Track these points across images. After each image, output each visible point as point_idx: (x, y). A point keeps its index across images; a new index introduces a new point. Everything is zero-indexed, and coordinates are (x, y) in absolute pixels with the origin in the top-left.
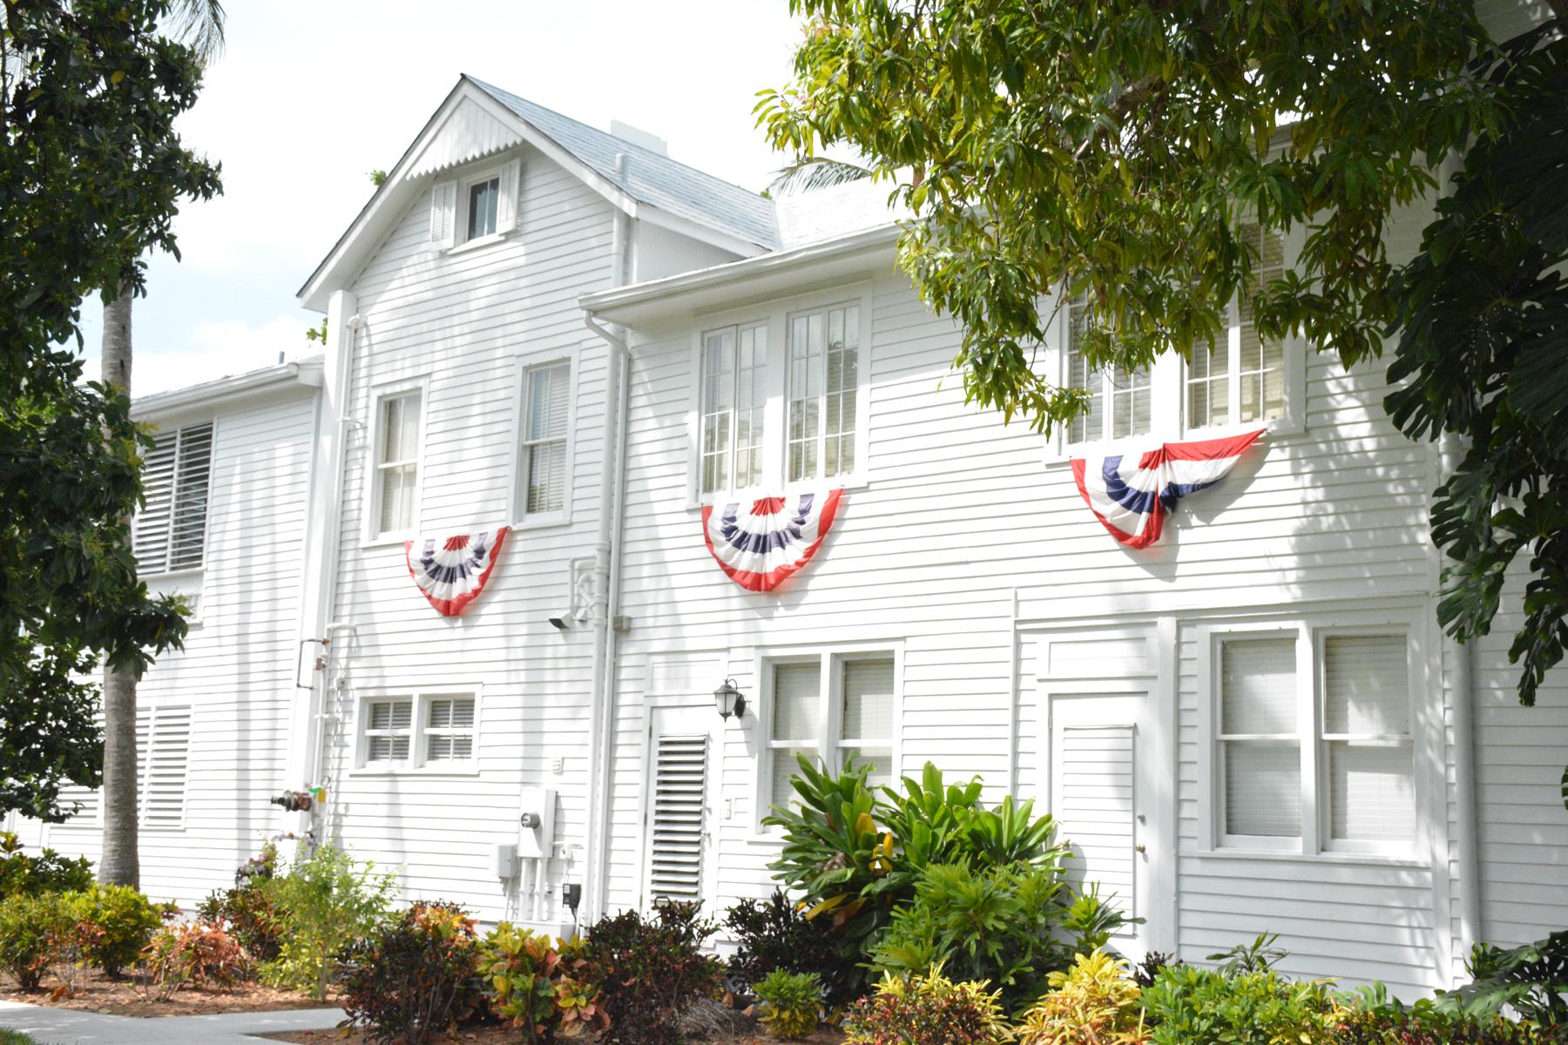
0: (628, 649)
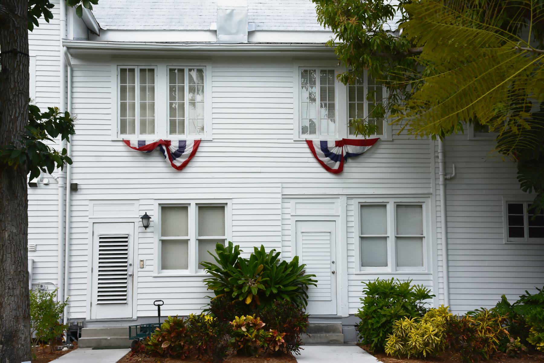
0: (76, 197)
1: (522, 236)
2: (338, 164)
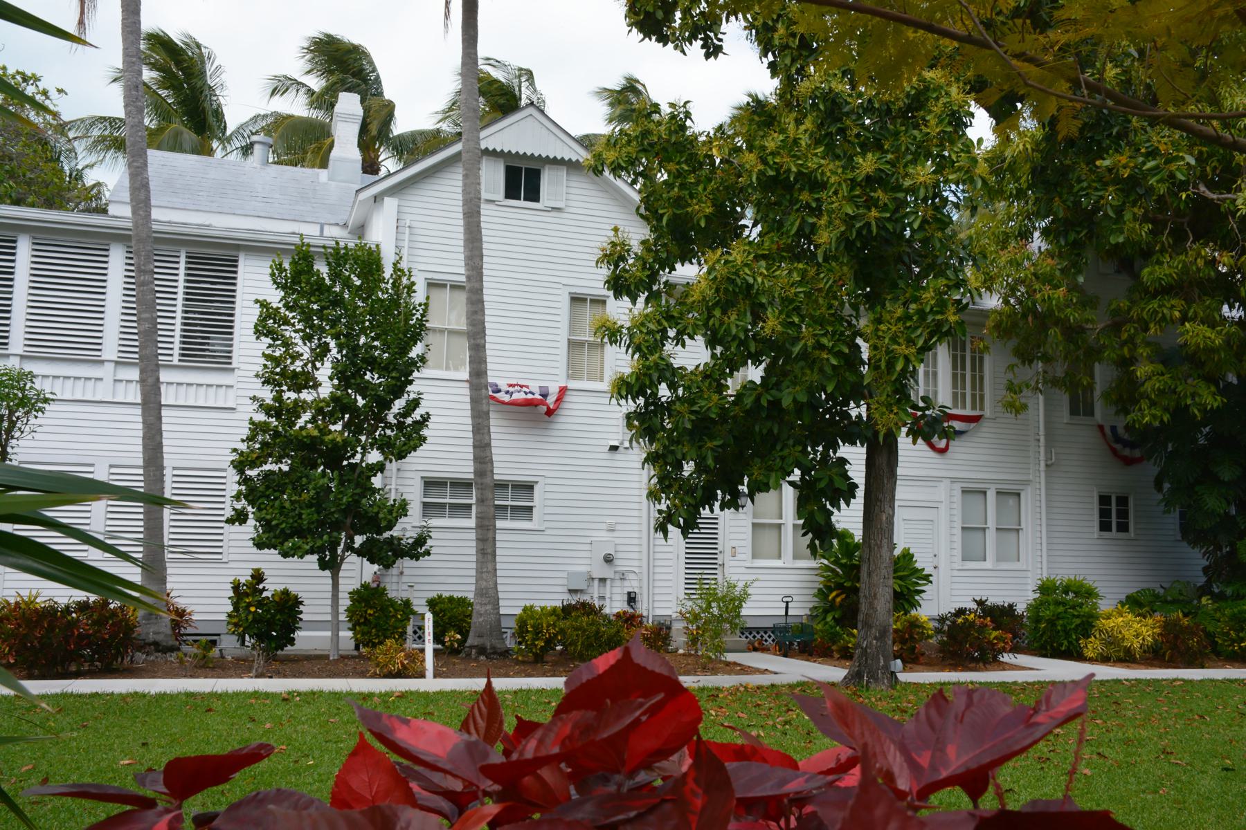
1: (1110, 530)
2: (944, 441)
